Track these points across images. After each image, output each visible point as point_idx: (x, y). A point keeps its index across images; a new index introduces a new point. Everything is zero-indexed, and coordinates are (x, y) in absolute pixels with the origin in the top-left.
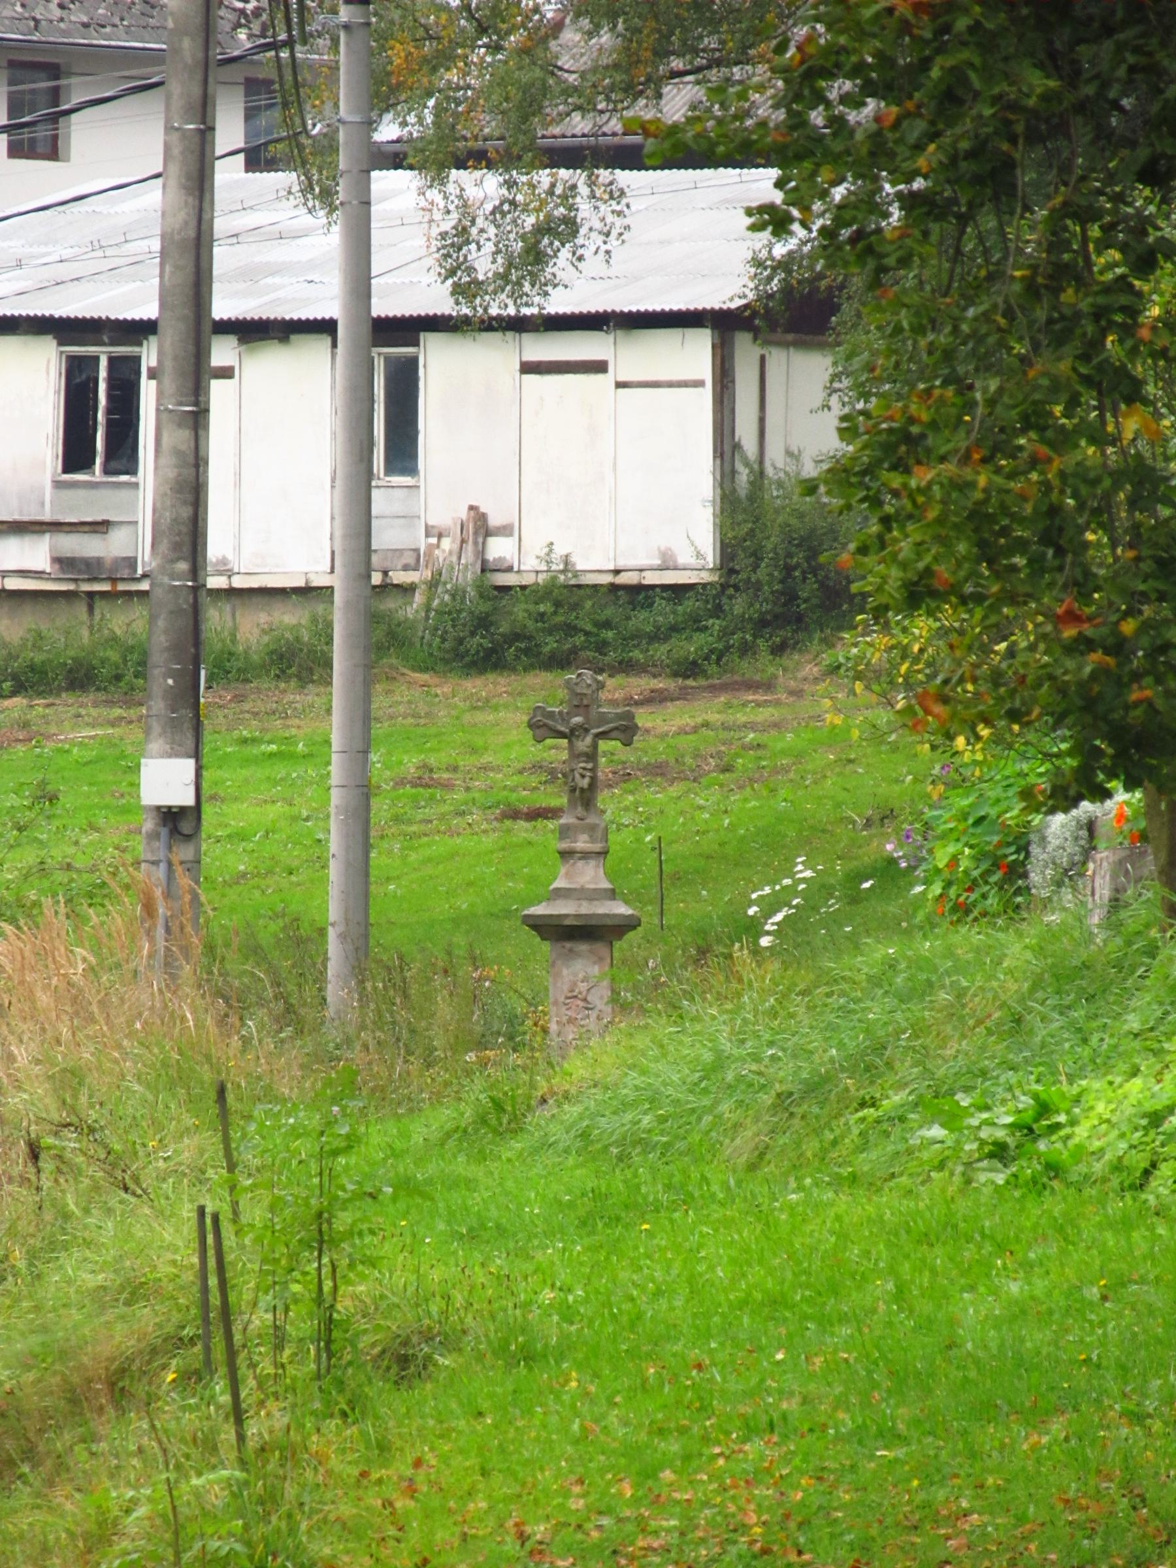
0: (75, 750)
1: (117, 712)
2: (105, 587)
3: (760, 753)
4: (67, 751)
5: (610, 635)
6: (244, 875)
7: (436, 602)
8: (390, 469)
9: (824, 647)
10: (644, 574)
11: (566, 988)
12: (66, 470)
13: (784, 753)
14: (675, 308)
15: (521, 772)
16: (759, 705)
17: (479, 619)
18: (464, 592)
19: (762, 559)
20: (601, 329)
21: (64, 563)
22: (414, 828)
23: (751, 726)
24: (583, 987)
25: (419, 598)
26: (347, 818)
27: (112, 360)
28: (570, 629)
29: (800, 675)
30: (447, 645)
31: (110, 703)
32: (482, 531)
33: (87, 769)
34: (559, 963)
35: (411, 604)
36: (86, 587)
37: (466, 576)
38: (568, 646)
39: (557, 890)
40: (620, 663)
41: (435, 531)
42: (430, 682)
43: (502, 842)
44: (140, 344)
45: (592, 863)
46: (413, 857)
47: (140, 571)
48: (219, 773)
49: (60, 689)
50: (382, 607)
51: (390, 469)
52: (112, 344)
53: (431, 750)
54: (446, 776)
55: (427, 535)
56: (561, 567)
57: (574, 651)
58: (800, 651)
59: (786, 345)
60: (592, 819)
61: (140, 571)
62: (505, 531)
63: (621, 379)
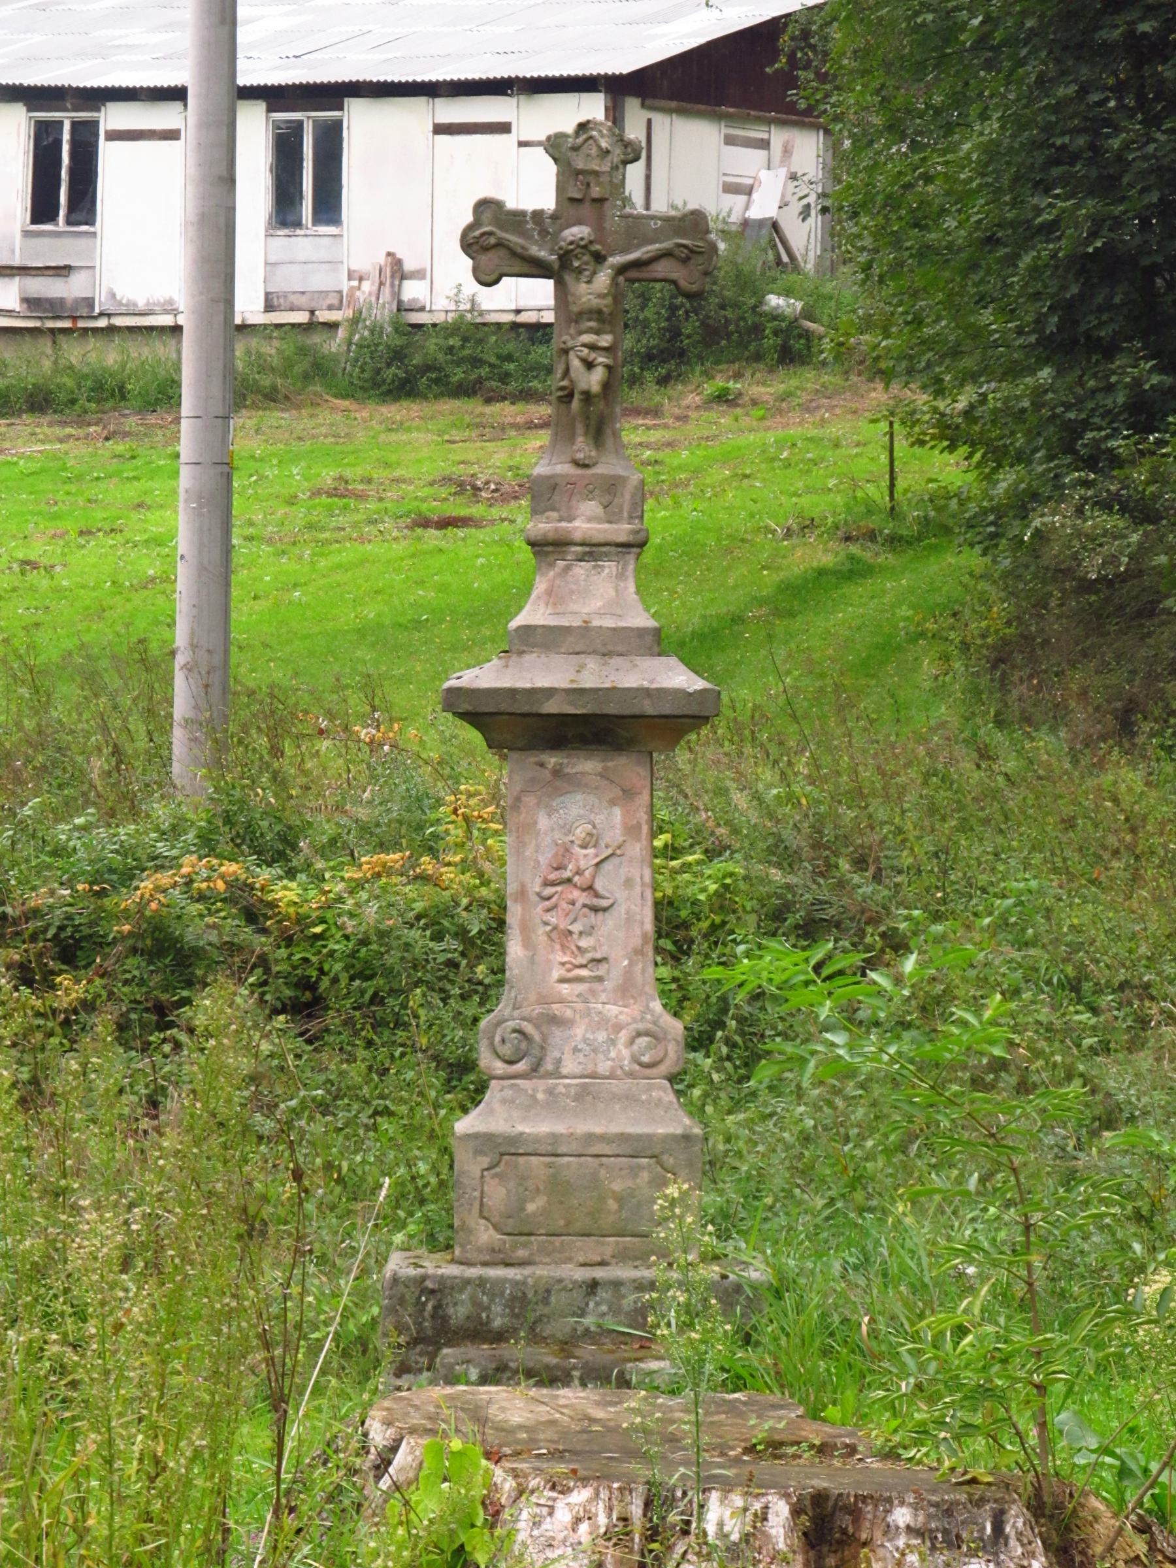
0: (21, 462)
1: (68, 430)
2: (67, 324)
3: (657, 468)
4: (16, 464)
5: (512, 367)
6: (153, 580)
7: (357, 337)
8: (317, 221)
9: (704, 379)
10: (543, 313)
11: (545, 859)
12: (35, 221)
13: (680, 468)
14: (573, 74)
15: (432, 484)
16: (649, 428)
17: (395, 352)
18: (382, 328)
19: (650, 299)
20: (506, 94)
21: (32, 303)
22: (327, 535)
23: (647, 446)
24: (585, 858)
25: (341, 333)
26: (200, 506)
27: (75, 125)
28: (476, 362)
29: (684, 403)
30: (366, 375)
31: (64, 424)
32: (398, 275)
33: (31, 479)
34: (530, 800)
35: (334, 338)
36: (50, 324)
37: (383, 313)
38: (473, 377)
39: (527, 631)
40: (521, 392)
41: (356, 275)
42: (352, 407)
43: (412, 549)
44: (99, 110)
45: (610, 567)
46: (323, 563)
47: (97, 311)
48: (150, 483)
49: (20, 413)
50: (309, 342)
51: (317, 221)
52: (75, 110)
53: (348, 464)
54: (360, 487)
55: (350, 278)
56: (468, 307)
57: (480, 381)
58: (682, 382)
59: (669, 111)
60: (607, 467)
61: (97, 311)
62: (419, 274)
63: (522, 139)
